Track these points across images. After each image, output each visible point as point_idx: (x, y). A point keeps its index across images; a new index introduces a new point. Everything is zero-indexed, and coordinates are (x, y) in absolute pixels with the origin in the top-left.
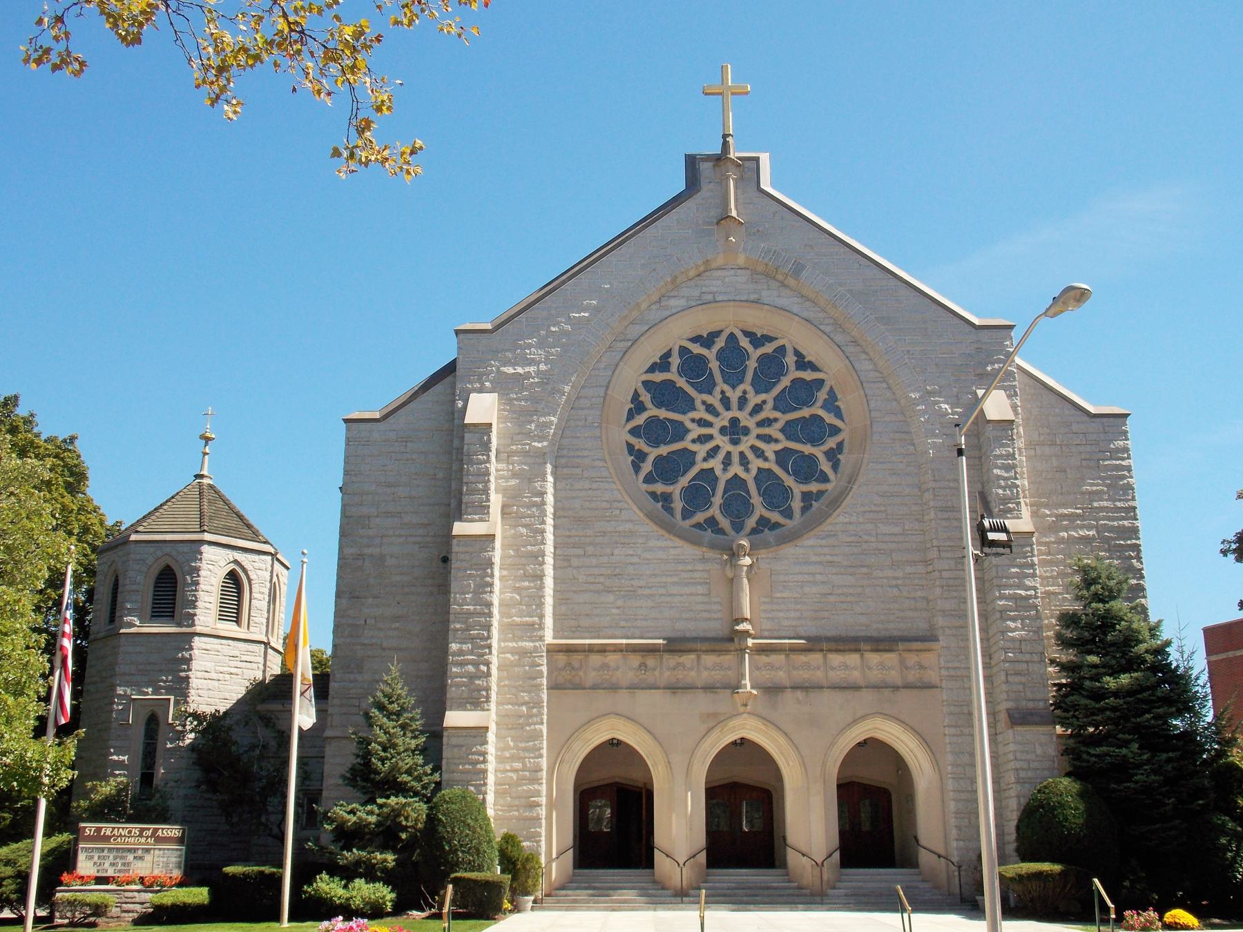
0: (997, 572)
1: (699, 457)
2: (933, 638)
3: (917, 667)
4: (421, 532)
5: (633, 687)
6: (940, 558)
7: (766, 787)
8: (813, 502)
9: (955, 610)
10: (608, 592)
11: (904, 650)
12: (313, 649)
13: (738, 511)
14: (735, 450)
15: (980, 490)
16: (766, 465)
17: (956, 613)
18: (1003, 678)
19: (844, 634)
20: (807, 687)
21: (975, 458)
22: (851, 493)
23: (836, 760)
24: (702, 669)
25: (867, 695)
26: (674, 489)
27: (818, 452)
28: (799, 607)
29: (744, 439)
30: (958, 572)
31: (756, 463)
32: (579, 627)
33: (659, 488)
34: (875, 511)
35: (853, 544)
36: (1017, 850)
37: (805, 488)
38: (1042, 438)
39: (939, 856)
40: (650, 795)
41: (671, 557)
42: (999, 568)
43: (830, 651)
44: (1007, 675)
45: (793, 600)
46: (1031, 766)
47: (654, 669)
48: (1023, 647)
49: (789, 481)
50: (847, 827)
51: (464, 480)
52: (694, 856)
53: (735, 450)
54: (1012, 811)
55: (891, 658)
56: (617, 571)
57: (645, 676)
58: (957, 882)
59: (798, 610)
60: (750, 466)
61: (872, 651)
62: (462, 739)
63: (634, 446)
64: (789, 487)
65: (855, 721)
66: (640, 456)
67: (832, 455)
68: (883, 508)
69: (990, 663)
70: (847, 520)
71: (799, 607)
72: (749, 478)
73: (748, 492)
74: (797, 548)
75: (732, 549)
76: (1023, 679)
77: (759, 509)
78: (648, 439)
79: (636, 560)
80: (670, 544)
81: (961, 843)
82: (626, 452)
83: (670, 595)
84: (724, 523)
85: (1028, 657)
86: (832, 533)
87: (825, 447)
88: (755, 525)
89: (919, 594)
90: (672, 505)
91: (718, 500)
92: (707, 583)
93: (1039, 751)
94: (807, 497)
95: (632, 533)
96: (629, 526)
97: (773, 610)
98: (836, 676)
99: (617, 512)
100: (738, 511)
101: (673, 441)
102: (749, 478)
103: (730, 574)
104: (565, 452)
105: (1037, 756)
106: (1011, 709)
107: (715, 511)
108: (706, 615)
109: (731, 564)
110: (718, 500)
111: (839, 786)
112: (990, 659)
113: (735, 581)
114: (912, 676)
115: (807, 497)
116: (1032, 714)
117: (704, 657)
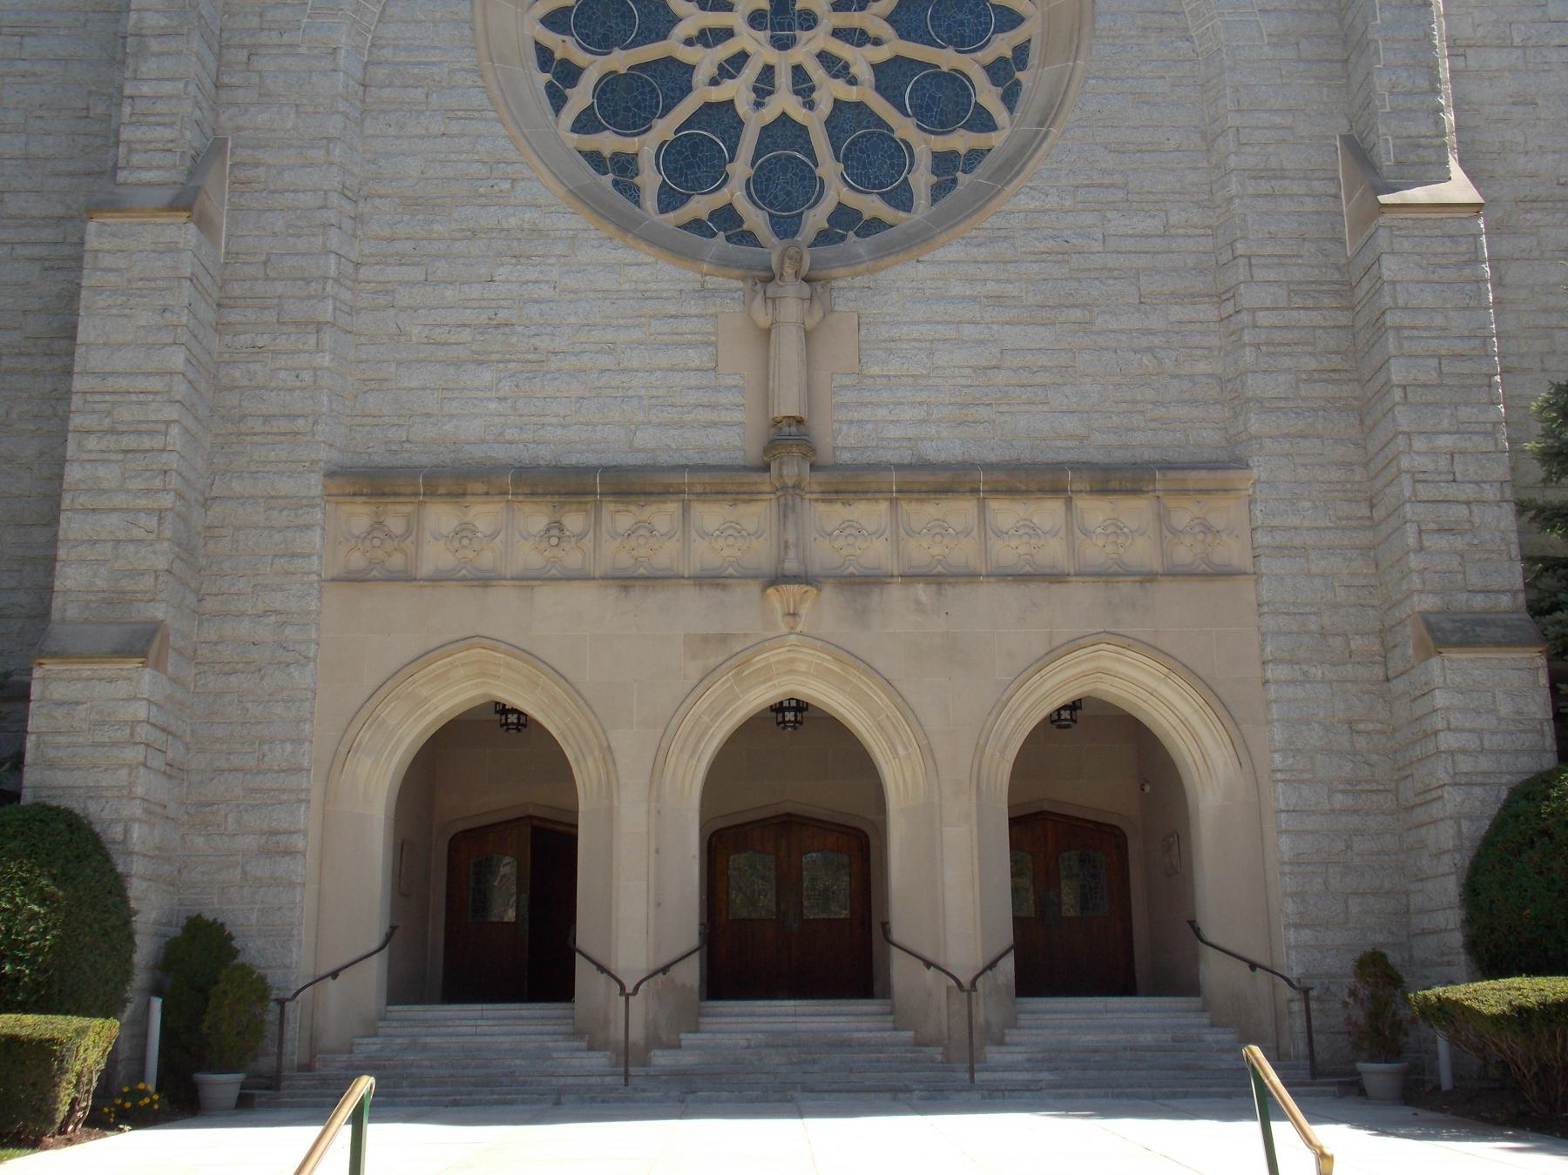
0: (1394, 298)
1: (700, 77)
2: (1241, 464)
3: (1197, 529)
4: (47, 234)
5: (528, 580)
6: (1251, 280)
7: (857, 824)
8: (959, 174)
9: (1286, 399)
10: (480, 363)
11: (1167, 491)
12: (767, 474)
13: (788, 193)
14: (783, 62)
15: (1345, 131)
16: (851, 94)
17: (1291, 404)
18: (1412, 540)
19: (1026, 456)
20: (939, 575)
21: (1331, 61)
22: (1045, 145)
23: (1006, 746)
24: (694, 534)
25: (1081, 595)
26: (642, 145)
27: (972, 65)
28: (923, 396)
29: (803, 36)
30: (1295, 314)
31: (830, 90)
32: (408, 441)
33: (608, 142)
34: (1100, 185)
35: (1053, 258)
36: (1472, 946)
37: (942, 143)
38: (1481, 32)
39: (1253, 966)
40: (573, 839)
41: (626, 286)
42: (1399, 287)
43: (995, 492)
44: (1420, 532)
45: (910, 380)
46: (1487, 744)
47: (581, 536)
48: (1458, 469)
49: (904, 128)
50: (1029, 910)
51: (128, 91)
52: (665, 970)
53: (783, 62)
54: (1439, 854)
55: (1135, 511)
56: (503, 315)
57: (556, 551)
58: (1299, 1023)
59: (921, 404)
60: (815, 95)
61: (1092, 492)
62: (80, 685)
63: (552, 53)
64: (904, 142)
65: (1054, 653)
66: (568, 74)
67: (1003, 73)
68: (1118, 179)
69: (1371, 518)
70: (1033, 205)
71: (923, 396)
72: (814, 122)
73: (811, 154)
74: (920, 266)
75: (769, 269)
76: (1459, 543)
77: (836, 188)
78: (585, 37)
79: (545, 291)
80: (629, 256)
81: (1306, 935)
82: (533, 62)
83: (624, 371)
84: (755, 219)
85: (1469, 491)
86: (1003, 233)
87: (988, 55)
88: (827, 226)
89: (1202, 367)
90: (637, 180)
91: (741, 169)
92: (708, 344)
93: (1505, 709)
94: (945, 163)
95: (537, 232)
96: (530, 215)
97: (861, 404)
98: (1008, 552)
99: (506, 185)
100: (788, 193)
101: (646, 37)
102: (814, 122)
103: (763, 320)
104: (387, 53)
105: (1500, 719)
106: (1430, 613)
107: (734, 192)
108: (704, 415)
109: (766, 299)
110: (741, 169)
111: (1014, 822)
112: (1372, 507)
113: (773, 335)
114: (1184, 553)
115: (945, 163)
116: (1484, 623)
117: (698, 508)
